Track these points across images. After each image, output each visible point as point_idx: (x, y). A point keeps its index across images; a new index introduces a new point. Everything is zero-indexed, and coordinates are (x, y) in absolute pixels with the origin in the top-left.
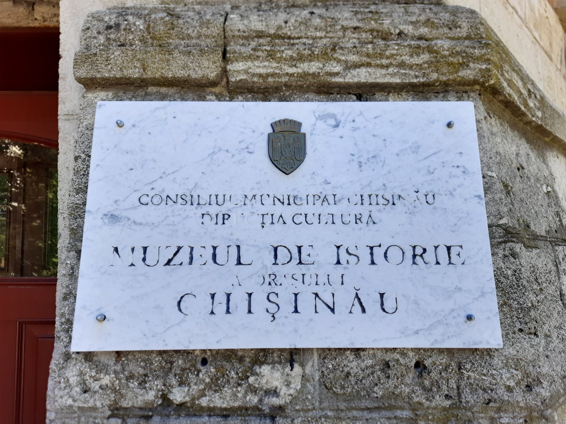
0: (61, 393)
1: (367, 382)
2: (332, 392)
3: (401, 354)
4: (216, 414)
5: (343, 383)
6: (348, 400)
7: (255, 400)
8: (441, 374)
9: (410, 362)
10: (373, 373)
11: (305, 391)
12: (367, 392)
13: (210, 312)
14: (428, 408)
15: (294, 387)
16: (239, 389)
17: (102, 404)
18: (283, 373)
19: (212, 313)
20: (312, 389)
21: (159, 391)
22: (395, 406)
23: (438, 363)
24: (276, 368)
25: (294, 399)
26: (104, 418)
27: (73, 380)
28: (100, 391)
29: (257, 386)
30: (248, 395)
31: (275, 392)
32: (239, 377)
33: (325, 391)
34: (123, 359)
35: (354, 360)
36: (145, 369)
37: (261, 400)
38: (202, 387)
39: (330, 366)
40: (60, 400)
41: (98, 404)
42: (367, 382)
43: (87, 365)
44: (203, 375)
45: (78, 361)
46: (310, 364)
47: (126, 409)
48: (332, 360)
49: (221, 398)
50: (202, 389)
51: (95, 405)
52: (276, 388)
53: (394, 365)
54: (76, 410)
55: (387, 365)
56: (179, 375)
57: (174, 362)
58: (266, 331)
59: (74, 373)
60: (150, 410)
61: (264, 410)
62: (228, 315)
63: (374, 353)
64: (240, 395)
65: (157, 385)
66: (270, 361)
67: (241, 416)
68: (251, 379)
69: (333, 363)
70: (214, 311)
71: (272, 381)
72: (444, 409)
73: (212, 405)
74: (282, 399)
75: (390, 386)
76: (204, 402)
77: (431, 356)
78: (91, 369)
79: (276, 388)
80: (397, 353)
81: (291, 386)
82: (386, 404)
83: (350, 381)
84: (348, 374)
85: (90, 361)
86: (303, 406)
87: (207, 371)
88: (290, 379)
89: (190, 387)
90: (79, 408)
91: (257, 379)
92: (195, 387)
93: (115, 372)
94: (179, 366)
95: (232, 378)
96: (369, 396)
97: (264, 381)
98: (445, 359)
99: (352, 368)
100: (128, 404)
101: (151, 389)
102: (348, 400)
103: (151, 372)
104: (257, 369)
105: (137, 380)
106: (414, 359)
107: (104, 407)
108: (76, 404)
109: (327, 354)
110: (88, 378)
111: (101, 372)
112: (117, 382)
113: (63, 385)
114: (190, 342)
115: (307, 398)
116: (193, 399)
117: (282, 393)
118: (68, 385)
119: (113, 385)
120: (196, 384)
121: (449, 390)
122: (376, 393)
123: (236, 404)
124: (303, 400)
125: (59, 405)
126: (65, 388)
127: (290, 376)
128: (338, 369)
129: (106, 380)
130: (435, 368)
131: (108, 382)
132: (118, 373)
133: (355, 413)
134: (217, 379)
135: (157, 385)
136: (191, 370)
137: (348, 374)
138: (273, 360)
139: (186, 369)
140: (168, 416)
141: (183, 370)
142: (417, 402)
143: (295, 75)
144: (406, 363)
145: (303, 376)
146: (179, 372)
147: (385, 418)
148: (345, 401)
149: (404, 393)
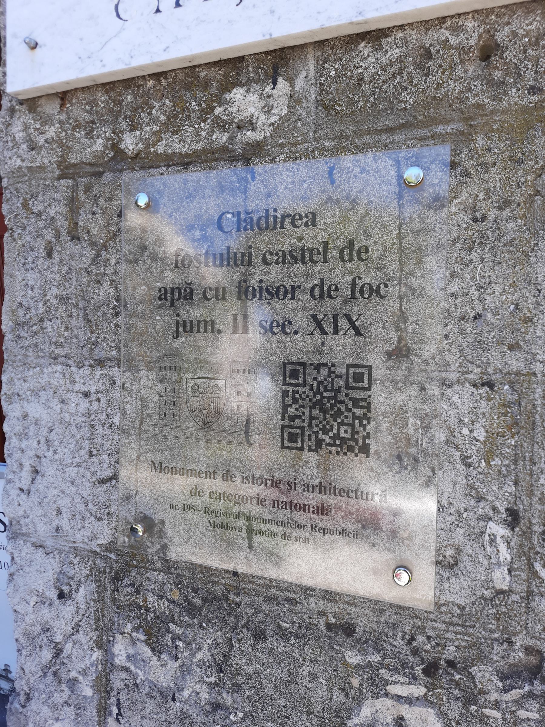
0: (10, 153)
1: (389, 88)
2: (334, 113)
3: (454, 31)
4: (175, 162)
5: (351, 97)
6: (357, 122)
7: (224, 138)
8: (525, 51)
9: (467, 39)
10: (400, 73)
11: (294, 117)
12: (390, 103)
13: (155, 11)
14: (493, 112)
15: (277, 113)
16: (203, 125)
17: (50, 162)
18: (262, 94)
19: (158, 11)
20: (304, 113)
21: (108, 140)
22: (435, 117)
23: (521, 32)
24: (252, 90)
25: (277, 128)
26: (53, 178)
27: (20, 136)
28: (46, 145)
29: (225, 118)
30: (215, 132)
31: (250, 124)
32: (203, 109)
33: (324, 114)
34: (68, 106)
35: (371, 54)
36: (91, 114)
37: (231, 139)
38: (156, 128)
39: (333, 73)
40: (9, 162)
41: (46, 161)
42: (389, 88)
43: (31, 116)
44: (157, 111)
45: (22, 114)
46: (302, 75)
47: (75, 165)
48: (335, 62)
49: (180, 141)
50: (158, 132)
51: (43, 164)
52: (252, 116)
53: (439, 51)
54: (26, 171)
55: (428, 55)
56: (130, 117)
57: (123, 101)
58: (229, 22)
59: (19, 128)
60: (101, 165)
61: (236, 150)
62: (179, 9)
63: (405, 37)
64: (203, 133)
65: (105, 132)
66: (244, 80)
67: (206, 162)
68: (218, 111)
69: (336, 67)
70: (160, 9)
71: (245, 107)
72: (525, 110)
73: (169, 152)
74: (260, 132)
75: (428, 87)
76: (160, 148)
77: (508, 23)
78: (35, 120)
79: (252, 116)
80: (446, 29)
81: (273, 111)
82: (420, 118)
83: (363, 91)
84: (361, 79)
85: (34, 112)
86: (290, 138)
87: (161, 106)
88: (272, 102)
89: (142, 130)
90: (30, 169)
91: (226, 109)
92: (148, 128)
93: (60, 122)
94: (128, 104)
95: (194, 111)
96: (392, 109)
97: (235, 109)
98: (535, 23)
99: (366, 68)
100: (76, 159)
101: (98, 138)
102: (357, 122)
103: (98, 118)
104: (227, 96)
105: (84, 130)
106: (476, 33)
107: (52, 164)
108: (24, 165)
109: (329, 55)
110: (32, 131)
111: (46, 124)
112: (64, 134)
113: (10, 144)
114: (132, 57)
115: (296, 127)
116: (147, 147)
117: (260, 124)
118: (16, 145)
119: (59, 137)
120: (148, 125)
121: (539, 77)
122: (405, 103)
123: (199, 146)
124: (290, 130)
125: (9, 168)
126: (13, 147)
127: (271, 98)
128: (344, 75)
129: (51, 132)
130: (515, 43)
131: (53, 134)
132: (64, 123)
133: (367, 139)
134: (176, 117)
135: (105, 132)
136: (143, 108)
137: (361, 79)
138: (248, 78)
139: (138, 108)
140: (121, 171)
141: (135, 110)
142: (474, 105)
143: (485, 11)
144: (460, 43)
145: (291, 97)
146: (129, 113)
147: (416, 138)
148: (354, 122)
149: (452, 93)
